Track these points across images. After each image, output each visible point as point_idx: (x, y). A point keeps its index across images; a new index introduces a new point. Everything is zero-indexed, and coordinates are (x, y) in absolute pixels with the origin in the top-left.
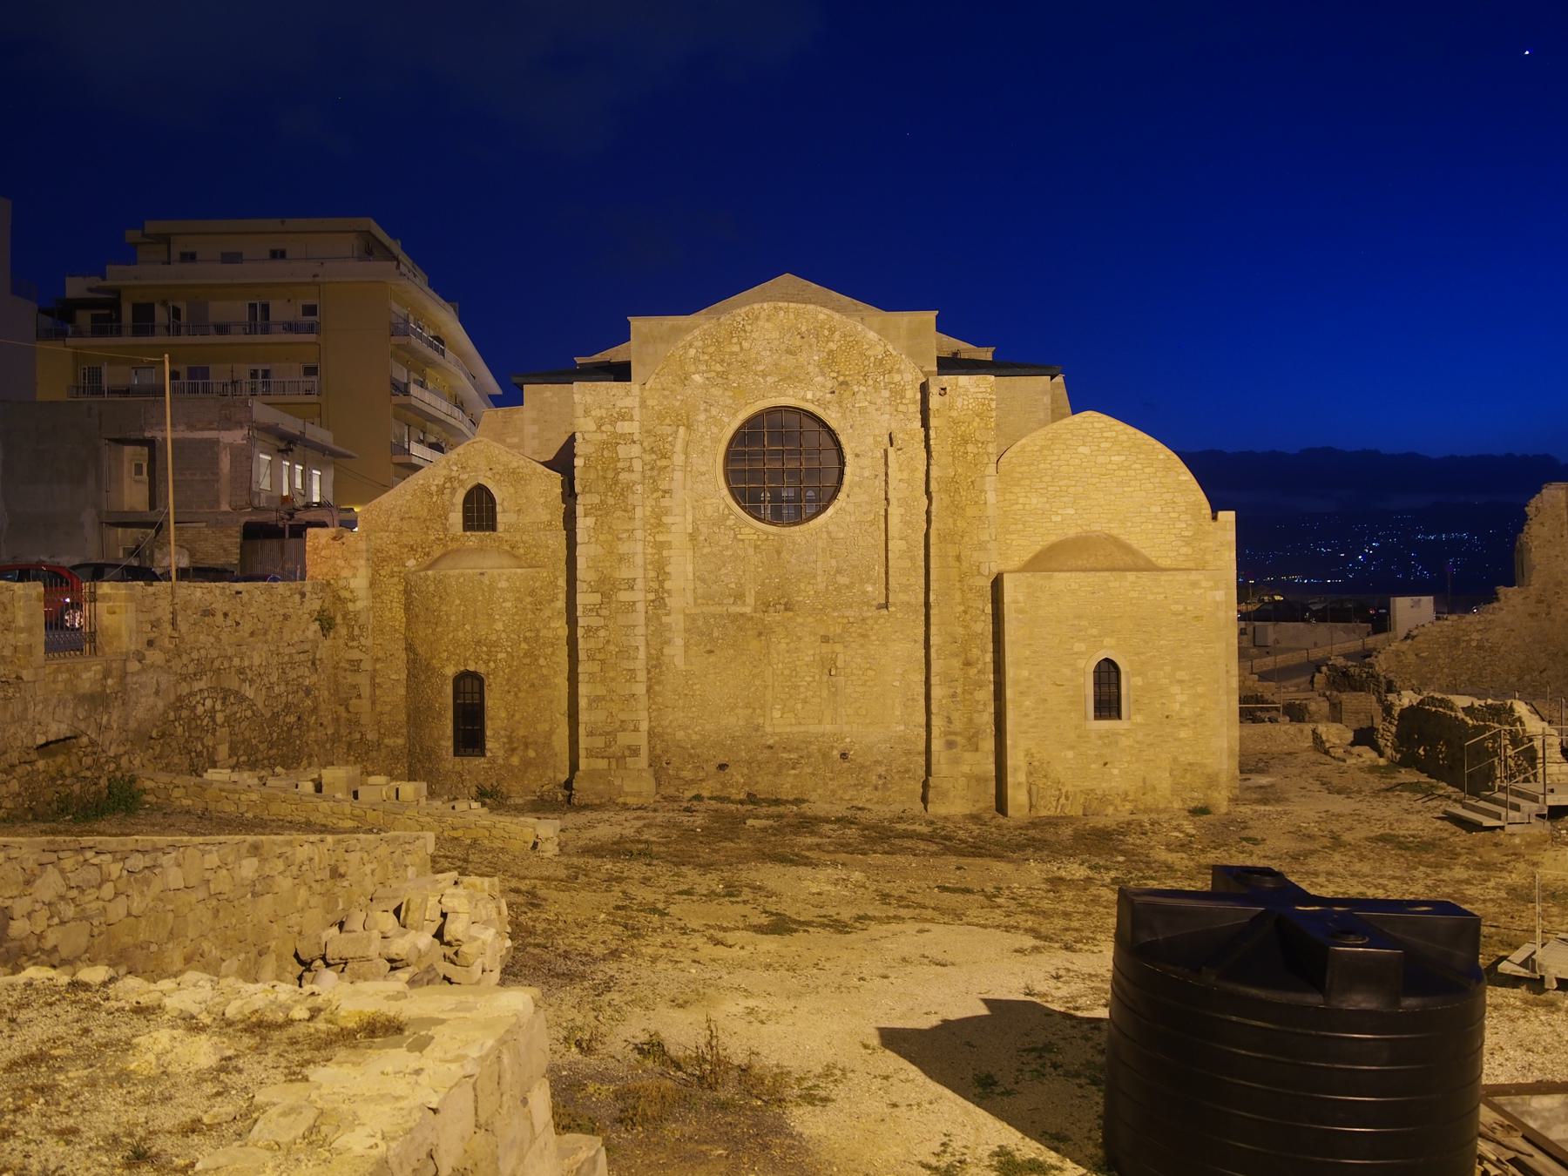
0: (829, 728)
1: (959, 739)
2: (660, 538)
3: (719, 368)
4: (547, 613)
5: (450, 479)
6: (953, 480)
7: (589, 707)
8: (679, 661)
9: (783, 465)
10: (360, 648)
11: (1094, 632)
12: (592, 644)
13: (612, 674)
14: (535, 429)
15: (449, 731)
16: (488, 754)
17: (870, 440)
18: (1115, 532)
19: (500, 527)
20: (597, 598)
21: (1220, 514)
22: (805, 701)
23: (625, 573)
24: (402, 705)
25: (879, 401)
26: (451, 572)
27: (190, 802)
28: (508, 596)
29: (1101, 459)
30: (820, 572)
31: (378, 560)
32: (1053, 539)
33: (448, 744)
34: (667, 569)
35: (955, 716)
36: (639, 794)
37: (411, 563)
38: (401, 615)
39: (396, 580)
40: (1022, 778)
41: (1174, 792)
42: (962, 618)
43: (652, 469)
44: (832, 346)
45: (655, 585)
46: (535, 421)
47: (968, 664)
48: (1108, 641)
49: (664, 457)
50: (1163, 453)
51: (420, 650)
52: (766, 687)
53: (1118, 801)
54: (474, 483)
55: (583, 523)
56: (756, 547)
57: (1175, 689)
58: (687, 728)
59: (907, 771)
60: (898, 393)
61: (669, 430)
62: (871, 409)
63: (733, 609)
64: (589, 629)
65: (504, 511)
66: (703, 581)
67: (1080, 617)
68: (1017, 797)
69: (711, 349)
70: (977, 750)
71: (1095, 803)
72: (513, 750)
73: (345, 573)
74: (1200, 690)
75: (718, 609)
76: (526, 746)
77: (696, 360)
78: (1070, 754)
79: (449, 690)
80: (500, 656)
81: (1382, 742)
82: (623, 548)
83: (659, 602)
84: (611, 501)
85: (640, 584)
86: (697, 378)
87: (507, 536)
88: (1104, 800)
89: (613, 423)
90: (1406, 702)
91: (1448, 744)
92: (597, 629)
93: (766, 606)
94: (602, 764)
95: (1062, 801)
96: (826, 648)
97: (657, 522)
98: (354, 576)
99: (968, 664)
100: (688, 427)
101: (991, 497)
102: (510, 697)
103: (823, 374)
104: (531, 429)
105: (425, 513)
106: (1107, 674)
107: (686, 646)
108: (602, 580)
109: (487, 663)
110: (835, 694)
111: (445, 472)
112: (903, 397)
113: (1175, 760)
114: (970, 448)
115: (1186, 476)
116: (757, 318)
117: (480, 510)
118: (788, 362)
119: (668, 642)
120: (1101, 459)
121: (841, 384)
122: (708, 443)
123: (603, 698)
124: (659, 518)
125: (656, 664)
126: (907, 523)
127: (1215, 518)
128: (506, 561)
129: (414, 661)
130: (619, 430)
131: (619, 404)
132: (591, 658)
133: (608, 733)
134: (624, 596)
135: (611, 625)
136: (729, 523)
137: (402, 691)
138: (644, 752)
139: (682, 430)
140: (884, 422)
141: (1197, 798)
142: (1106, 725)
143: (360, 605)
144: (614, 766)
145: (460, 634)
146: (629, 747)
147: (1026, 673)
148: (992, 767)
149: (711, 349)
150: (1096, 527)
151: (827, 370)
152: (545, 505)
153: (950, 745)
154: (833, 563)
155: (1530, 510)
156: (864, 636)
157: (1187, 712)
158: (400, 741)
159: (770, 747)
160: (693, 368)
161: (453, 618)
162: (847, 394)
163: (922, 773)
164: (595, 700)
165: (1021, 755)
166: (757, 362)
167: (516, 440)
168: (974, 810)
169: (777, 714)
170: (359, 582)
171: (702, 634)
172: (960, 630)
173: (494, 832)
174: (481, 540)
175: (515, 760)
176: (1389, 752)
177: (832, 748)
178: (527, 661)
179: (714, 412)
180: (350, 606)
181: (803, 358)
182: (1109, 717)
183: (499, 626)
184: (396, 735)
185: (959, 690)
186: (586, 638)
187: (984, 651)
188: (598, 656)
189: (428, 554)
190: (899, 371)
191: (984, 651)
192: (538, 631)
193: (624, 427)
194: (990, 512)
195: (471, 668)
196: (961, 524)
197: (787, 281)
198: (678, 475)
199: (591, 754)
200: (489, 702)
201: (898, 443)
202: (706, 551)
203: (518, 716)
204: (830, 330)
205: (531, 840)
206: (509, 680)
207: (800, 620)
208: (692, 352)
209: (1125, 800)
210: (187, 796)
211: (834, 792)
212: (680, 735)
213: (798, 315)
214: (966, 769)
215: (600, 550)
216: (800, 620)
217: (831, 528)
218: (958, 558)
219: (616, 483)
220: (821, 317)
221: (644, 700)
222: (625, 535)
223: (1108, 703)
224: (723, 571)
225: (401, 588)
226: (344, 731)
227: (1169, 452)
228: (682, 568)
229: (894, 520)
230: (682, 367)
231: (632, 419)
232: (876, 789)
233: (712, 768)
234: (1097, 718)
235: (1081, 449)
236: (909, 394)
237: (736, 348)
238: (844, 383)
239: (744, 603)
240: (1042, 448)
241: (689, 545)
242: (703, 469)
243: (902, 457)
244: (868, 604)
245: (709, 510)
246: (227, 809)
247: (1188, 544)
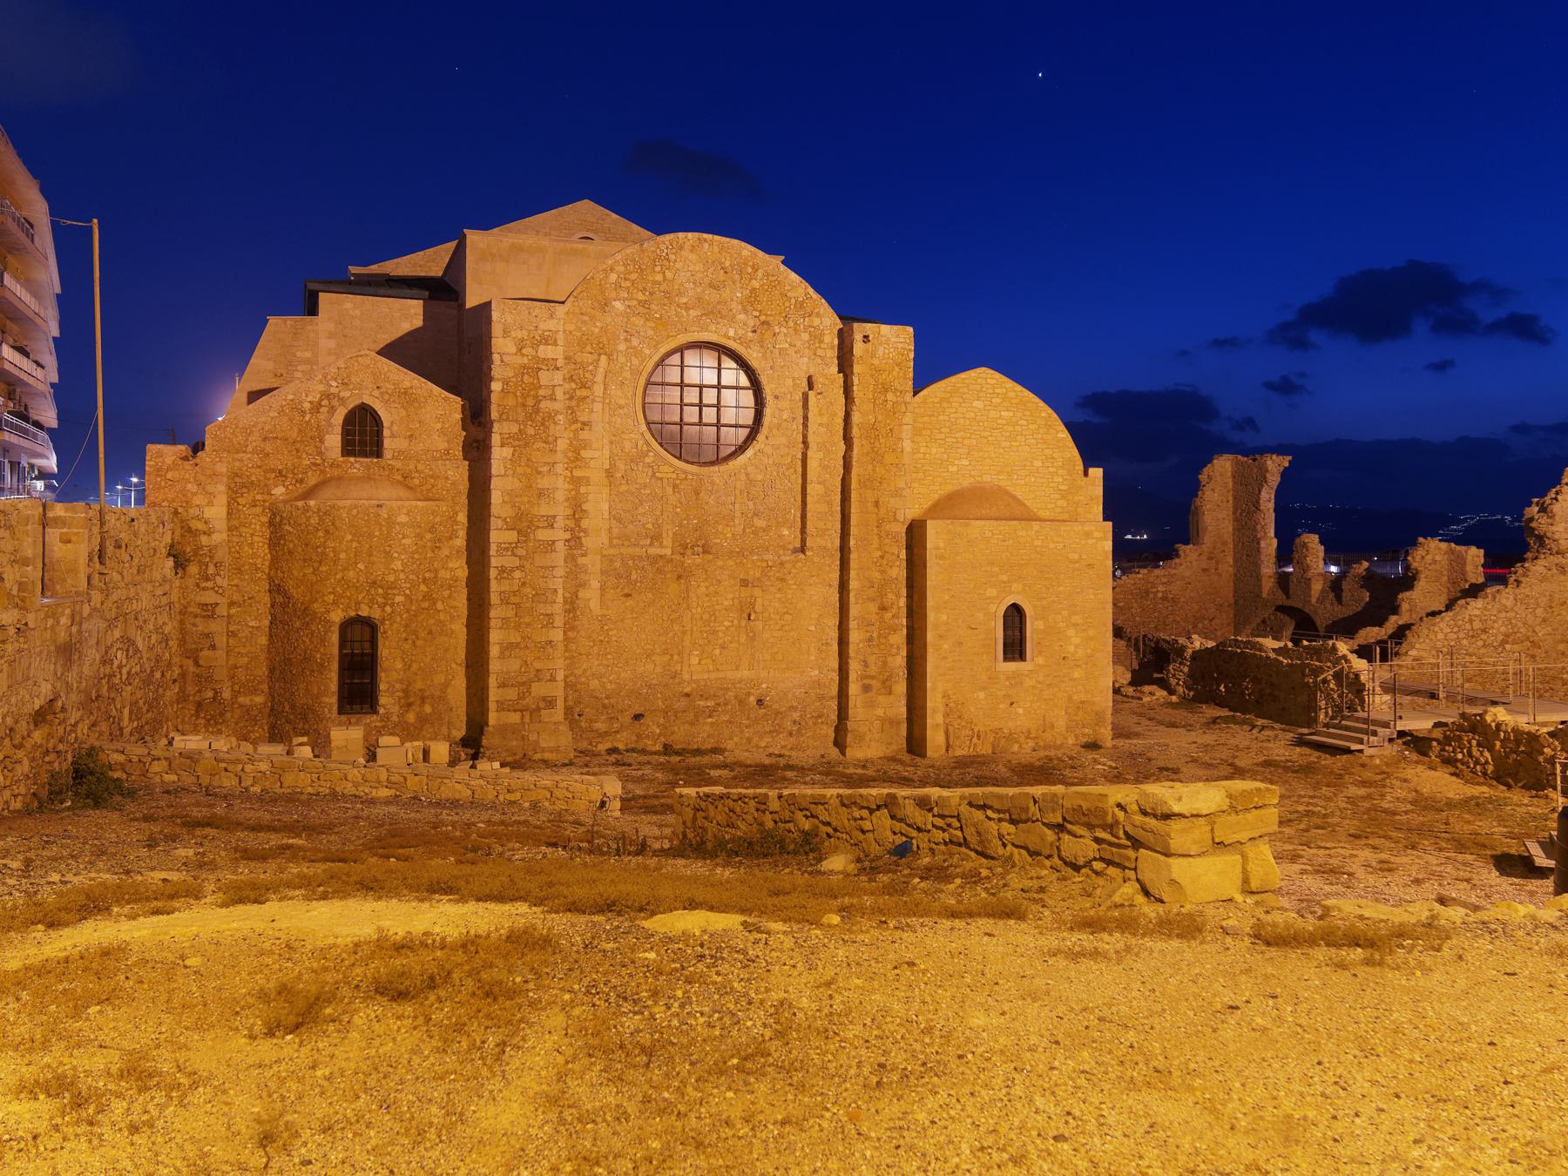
0: (745, 673)
2: (577, 473)
3: (641, 297)
4: (446, 552)
5: (328, 396)
6: (873, 427)
7: (502, 657)
8: (594, 605)
10: (217, 589)
11: (1005, 578)
12: (505, 587)
13: (527, 620)
14: (332, 344)
15: (334, 686)
16: (382, 711)
17: (789, 382)
18: (1002, 484)
19: (387, 454)
20: (512, 536)
21: (1091, 470)
22: (723, 647)
23: (544, 509)
24: (263, 657)
25: (798, 344)
26: (341, 503)
27: (174, 778)
28: (408, 531)
29: (993, 414)
30: (738, 514)
31: (238, 486)
32: (950, 488)
33: (333, 700)
35: (871, 659)
36: (556, 750)
37: (279, 491)
38: (264, 551)
39: (258, 510)
40: (939, 719)
41: (1069, 729)
42: (880, 564)
43: (571, 398)
44: (755, 284)
45: (571, 524)
46: (331, 335)
47: (883, 608)
48: (1015, 587)
49: (584, 386)
50: (1045, 411)
51: (293, 592)
52: (684, 633)
53: (1022, 739)
54: (358, 402)
55: (499, 455)
56: (675, 486)
57: (1071, 632)
58: (602, 676)
59: (820, 716)
60: (817, 337)
61: (590, 358)
62: (791, 351)
63: (652, 551)
64: (502, 570)
65: (393, 436)
66: (620, 521)
67: (992, 564)
68: (935, 739)
69: (634, 276)
70: (890, 693)
71: (1002, 742)
72: (409, 705)
73: (197, 500)
74: (1091, 633)
75: (637, 551)
76: (423, 700)
77: (617, 286)
78: (982, 695)
79: (335, 638)
81: (1173, 681)
82: (543, 483)
83: (575, 541)
85: (560, 523)
86: (618, 304)
87: (398, 464)
88: (1010, 738)
89: (535, 346)
90: (1197, 645)
91: (1255, 680)
92: (512, 570)
93: (684, 548)
94: (514, 718)
95: (975, 740)
96: (745, 593)
97: (576, 456)
98: (210, 504)
99: (883, 608)
100: (609, 356)
101: (907, 445)
102: (407, 646)
103: (745, 311)
104: (326, 344)
105: (294, 434)
106: (1015, 616)
107: (602, 589)
108: (520, 516)
109: (383, 606)
110: (753, 639)
111: (321, 388)
112: (821, 342)
113: (1070, 698)
114: (890, 396)
115: (1064, 434)
116: (681, 248)
117: (363, 433)
118: (711, 296)
119: (583, 585)
120: (993, 414)
121: (763, 323)
122: (627, 374)
124: (577, 452)
125: (572, 606)
126: (826, 468)
127: (1086, 474)
128: (402, 492)
129: (284, 606)
130: (541, 355)
131: (542, 326)
132: (505, 601)
133: (523, 684)
135: (528, 566)
136: (647, 460)
137: (263, 640)
138: (560, 704)
139: (604, 359)
140: (804, 365)
141: (1088, 734)
142: (1013, 666)
144: (527, 719)
145: (351, 574)
146: (544, 699)
147: (944, 617)
148: (904, 710)
149: (634, 276)
150: (987, 478)
151: (749, 308)
152: (442, 432)
153: (866, 688)
154: (751, 504)
155: (1203, 477)
156: (782, 580)
157: (1080, 653)
158: (259, 699)
159: (687, 695)
160: (613, 294)
161: (343, 556)
162: (768, 335)
163: (834, 717)
164: (508, 648)
165: (939, 696)
166: (680, 294)
167: (308, 355)
168: (889, 752)
169: (694, 660)
170: (216, 512)
171: (618, 576)
172: (877, 575)
173: (557, 793)
174: (368, 467)
175: (411, 717)
176: (1180, 690)
177: (749, 694)
178: (426, 605)
179: (635, 342)
180: (204, 539)
181: (726, 294)
182: (1013, 660)
183: (398, 565)
184: (254, 691)
185: (875, 635)
186: (499, 579)
187: (898, 596)
188: (513, 599)
189: (301, 481)
190: (818, 315)
191: (898, 596)
192: (436, 571)
193: (546, 352)
194: (906, 459)
195: (364, 612)
196: (880, 470)
197: (586, 210)
198: (598, 407)
199: (502, 706)
200: (384, 651)
201: (818, 387)
202: (624, 488)
203: (415, 667)
204: (753, 267)
205: (597, 798)
206: (406, 626)
207: (720, 563)
208: (613, 277)
209: (1028, 738)
210: (170, 769)
211: (749, 740)
212: (594, 684)
213: (722, 249)
214: (880, 712)
215: (517, 484)
216: (720, 563)
217: (750, 469)
218: (877, 504)
219: (537, 411)
221: (561, 647)
222: (545, 469)
223: (1015, 648)
224: (641, 510)
225: (265, 519)
226: (191, 689)
227: (1050, 411)
228: (599, 505)
229: (813, 465)
230: (602, 292)
231: (555, 343)
232: (791, 734)
233: (626, 719)
234: (1006, 659)
235: (976, 403)
236: (827, 339)
237: (659, 277)
239: (661, 546)
240: (942, 400)
241: (606, 482)
242: (622, 402)
244: (784, 548)
245: (628, 446)
246: (226, 783)
247: (1063, 497)
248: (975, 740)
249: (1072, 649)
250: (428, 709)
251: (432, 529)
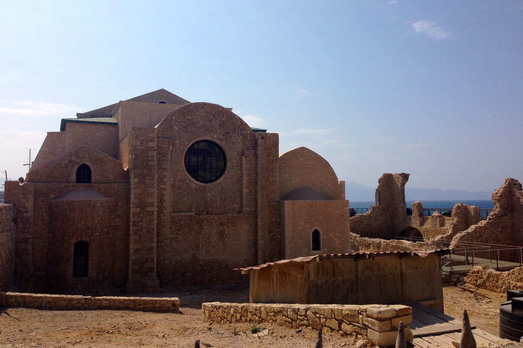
2: (162, 187)
3: (184, 124)
16: (89, 275)
20: (138, 210)
22: (213, 247)
23: (150, 200)
29: (306, 163)
34: (164, 198)
49: (164, 156)
66: (176, 203)
80: (96, 234)
83: (160, 211)
92: (138, 222)
97: (161, 181)
98: (27, 201)
106: (316, 234)
114: (271, 157)
118: (208, 124)
120: (306, 163)
121: (226, 133)
123: (140, 249)
131: (149, 135)
136: (187, 181)
143: (29, 214)
149: (181, 118)
151: (222, 128)
157: (339, 247)
159: (201, 265)
166: (198, 123)
169: (203, 253)
175: (100, 277)
183: (96, 222)
222: (150, 186)
231: (154, 141)
237: (190, 118)
239: (192, 212)
243: (248, 160)
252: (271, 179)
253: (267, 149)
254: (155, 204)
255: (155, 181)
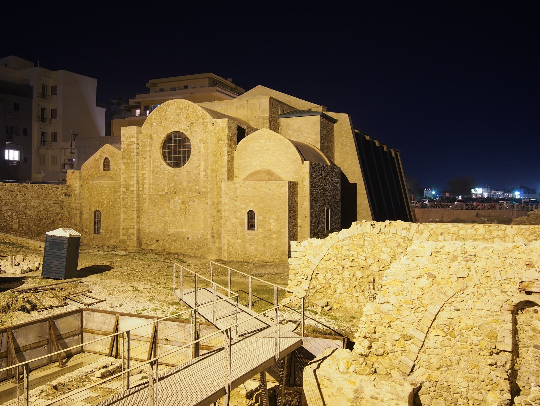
1: (215, 235)
7: (123, 221)
9: (176, 150)
23: (132, 182)
28: (107, 189)
40: (226, 248)
41: (272, 256)
44: (189, 112)
48: (252, 204)
49: (144, 148)
76: (111, 232)
84: (129, 161)
86: (154, 124)
94: (126, 238)
106: (251, 215)
108: (127, 184)
114: (220, 142)
119: (144, 203)
127: (303, 163)
134: (131, 189)
142: (250, 232)
175: (108, 236)
181: (181, 115)
183: (104, 197)
213: (180, 103)
218: (216, 177)
220: (186, 103)
223: (251, 226)
228: (148, 181)
233: (154, 241)
237: (164, 114)
238: (192, 123)
248: (237, 256)
249: (272, 227)
250: (113, 234)
251: (114, 188)
252: (219, 163)
253: (216, 134)
254: (135, 185)
255: (135, 168)
